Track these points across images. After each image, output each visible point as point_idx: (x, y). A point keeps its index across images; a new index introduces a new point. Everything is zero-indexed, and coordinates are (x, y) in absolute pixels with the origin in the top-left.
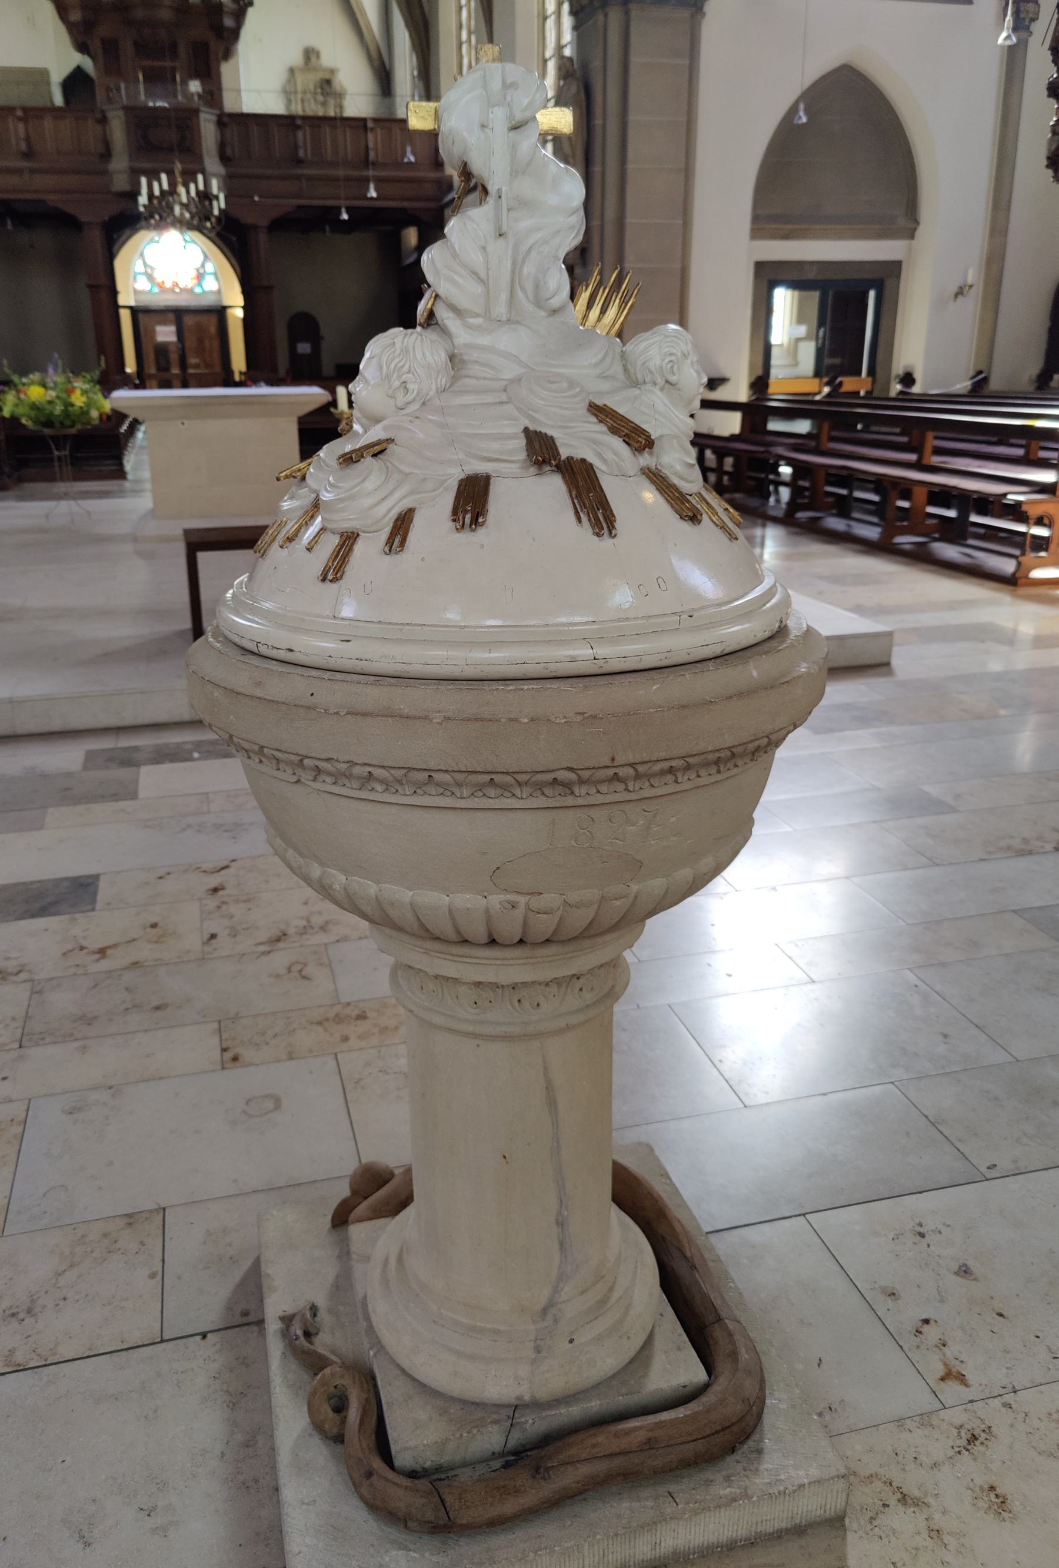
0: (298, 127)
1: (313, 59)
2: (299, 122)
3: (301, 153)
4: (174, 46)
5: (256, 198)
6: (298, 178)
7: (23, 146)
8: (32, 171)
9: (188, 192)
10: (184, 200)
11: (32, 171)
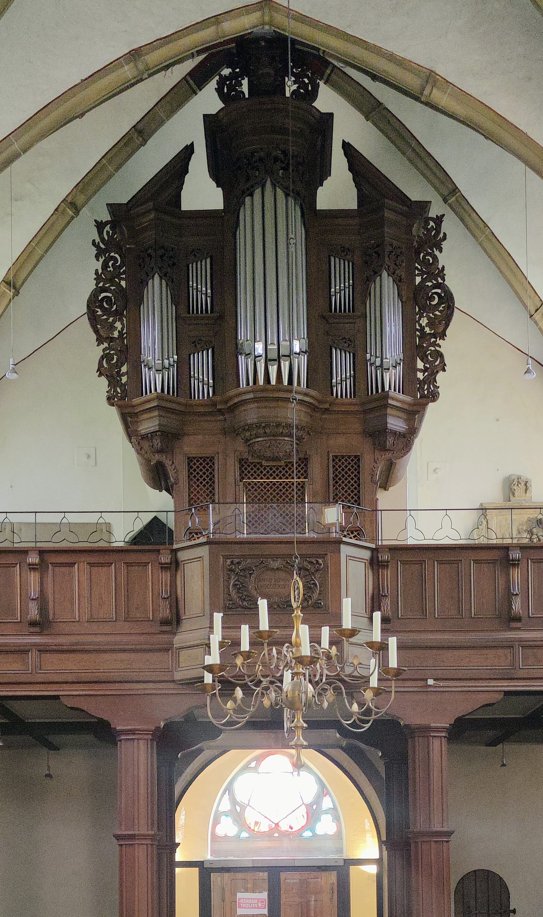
0: (515, 564)
1: (519, 491)
2: (515, 554)
3: (517, 606)
4: (304, 461)
5: (431, 682)
6: (509, 646)
7: (34, 612)
8: (43, 650)
9: (315, 640)
10: (306, 650)
11: (43, 650)
